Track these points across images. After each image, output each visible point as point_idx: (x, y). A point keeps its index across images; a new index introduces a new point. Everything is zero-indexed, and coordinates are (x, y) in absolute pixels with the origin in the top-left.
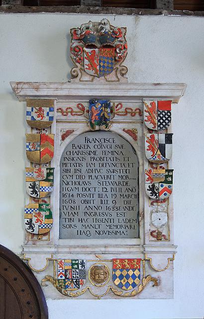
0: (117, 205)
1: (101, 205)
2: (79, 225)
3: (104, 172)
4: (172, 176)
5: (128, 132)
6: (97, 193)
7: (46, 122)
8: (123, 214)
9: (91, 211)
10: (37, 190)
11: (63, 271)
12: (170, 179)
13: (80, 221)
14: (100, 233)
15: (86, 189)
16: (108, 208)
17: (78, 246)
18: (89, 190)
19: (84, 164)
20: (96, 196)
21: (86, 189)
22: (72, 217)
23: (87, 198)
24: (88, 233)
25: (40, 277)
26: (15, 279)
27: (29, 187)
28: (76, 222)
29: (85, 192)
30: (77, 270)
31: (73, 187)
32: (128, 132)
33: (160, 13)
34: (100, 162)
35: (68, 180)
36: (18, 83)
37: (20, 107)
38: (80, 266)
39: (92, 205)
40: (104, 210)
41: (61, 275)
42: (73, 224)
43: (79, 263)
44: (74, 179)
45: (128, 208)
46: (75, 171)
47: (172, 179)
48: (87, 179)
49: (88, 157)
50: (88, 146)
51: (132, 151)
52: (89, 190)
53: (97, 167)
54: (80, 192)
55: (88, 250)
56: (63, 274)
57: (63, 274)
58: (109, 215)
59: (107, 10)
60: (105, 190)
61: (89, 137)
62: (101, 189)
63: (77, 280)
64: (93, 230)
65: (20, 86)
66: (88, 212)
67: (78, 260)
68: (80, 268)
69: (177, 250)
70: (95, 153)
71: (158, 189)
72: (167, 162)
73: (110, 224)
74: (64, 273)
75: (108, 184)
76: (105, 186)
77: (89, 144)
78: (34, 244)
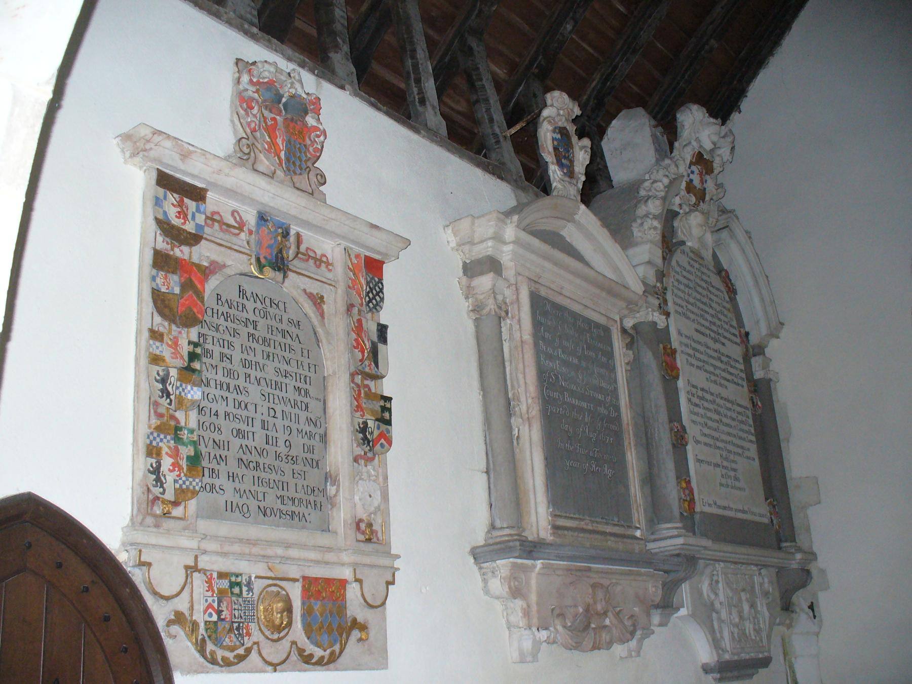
0: (293, 453)
1: (267, 447)
2: (229, 486)
3: (270, 373)
4: (389, 410)
5: (311, 296)
6: (258, 417)
7: (190, 233)
8: (302, 473)
9: (251, 458)
10: (170, 388)
11: (214, 601)
12: (387, 415)
13: (231, 479)
14: (265, 511)
15: (240, 404)
16: (278, 456)
17: (241, 540)
18: (246, 406)
19: (237, 343)
20: (258, 424)
21: (240, 404)
22: (217, 467)
23: (243, 427)
24: (245, 508)
25: (160, 613)
26: (107, 619)
27: (157, 381)
28: (222, 481)
29: (239, 412)
30: (240, 600)
31: (218, 393)
32: (311, 296)
33: (342, 87)
34: (263, 347)
35: (209, 376)
36: (157, 132)
37: (137, 181)
38: (245, 589)
39: (250, 443)
40: (269, 460)
41: (210, 610)
42: (217, 482)
43: (244, 581)
44: (220, 377)
45: (310, 461)
46: (222, 355)
47: (390, 416)
48: (241, 382)
49: (244, 331)
50: (244, 306)
51: (314, 340)
52: (246, 406)
53: (259, 358)
54: (230, 409)
55: (255, 550)
56: (213, 608)
57: (213, 608)
58: (280, 472)
59: (269, 41)
60: (272, 412)
61: (245, 287)
62: (265, 412)
63: (239, 623)
64: (253, 504)
65: (157, 139)
66: (244, 458)
67: (241, 575)
68: (245, 594)
69: (397, 564)
70: (255, 325)
71: (372, 433)
72: (378, 377)
73: (282, 493)
74: (215, 605)
75: (277, 401)
76: (272, 406)
77: (245, 302)
78: (157, 526)
